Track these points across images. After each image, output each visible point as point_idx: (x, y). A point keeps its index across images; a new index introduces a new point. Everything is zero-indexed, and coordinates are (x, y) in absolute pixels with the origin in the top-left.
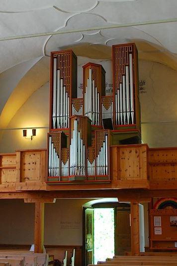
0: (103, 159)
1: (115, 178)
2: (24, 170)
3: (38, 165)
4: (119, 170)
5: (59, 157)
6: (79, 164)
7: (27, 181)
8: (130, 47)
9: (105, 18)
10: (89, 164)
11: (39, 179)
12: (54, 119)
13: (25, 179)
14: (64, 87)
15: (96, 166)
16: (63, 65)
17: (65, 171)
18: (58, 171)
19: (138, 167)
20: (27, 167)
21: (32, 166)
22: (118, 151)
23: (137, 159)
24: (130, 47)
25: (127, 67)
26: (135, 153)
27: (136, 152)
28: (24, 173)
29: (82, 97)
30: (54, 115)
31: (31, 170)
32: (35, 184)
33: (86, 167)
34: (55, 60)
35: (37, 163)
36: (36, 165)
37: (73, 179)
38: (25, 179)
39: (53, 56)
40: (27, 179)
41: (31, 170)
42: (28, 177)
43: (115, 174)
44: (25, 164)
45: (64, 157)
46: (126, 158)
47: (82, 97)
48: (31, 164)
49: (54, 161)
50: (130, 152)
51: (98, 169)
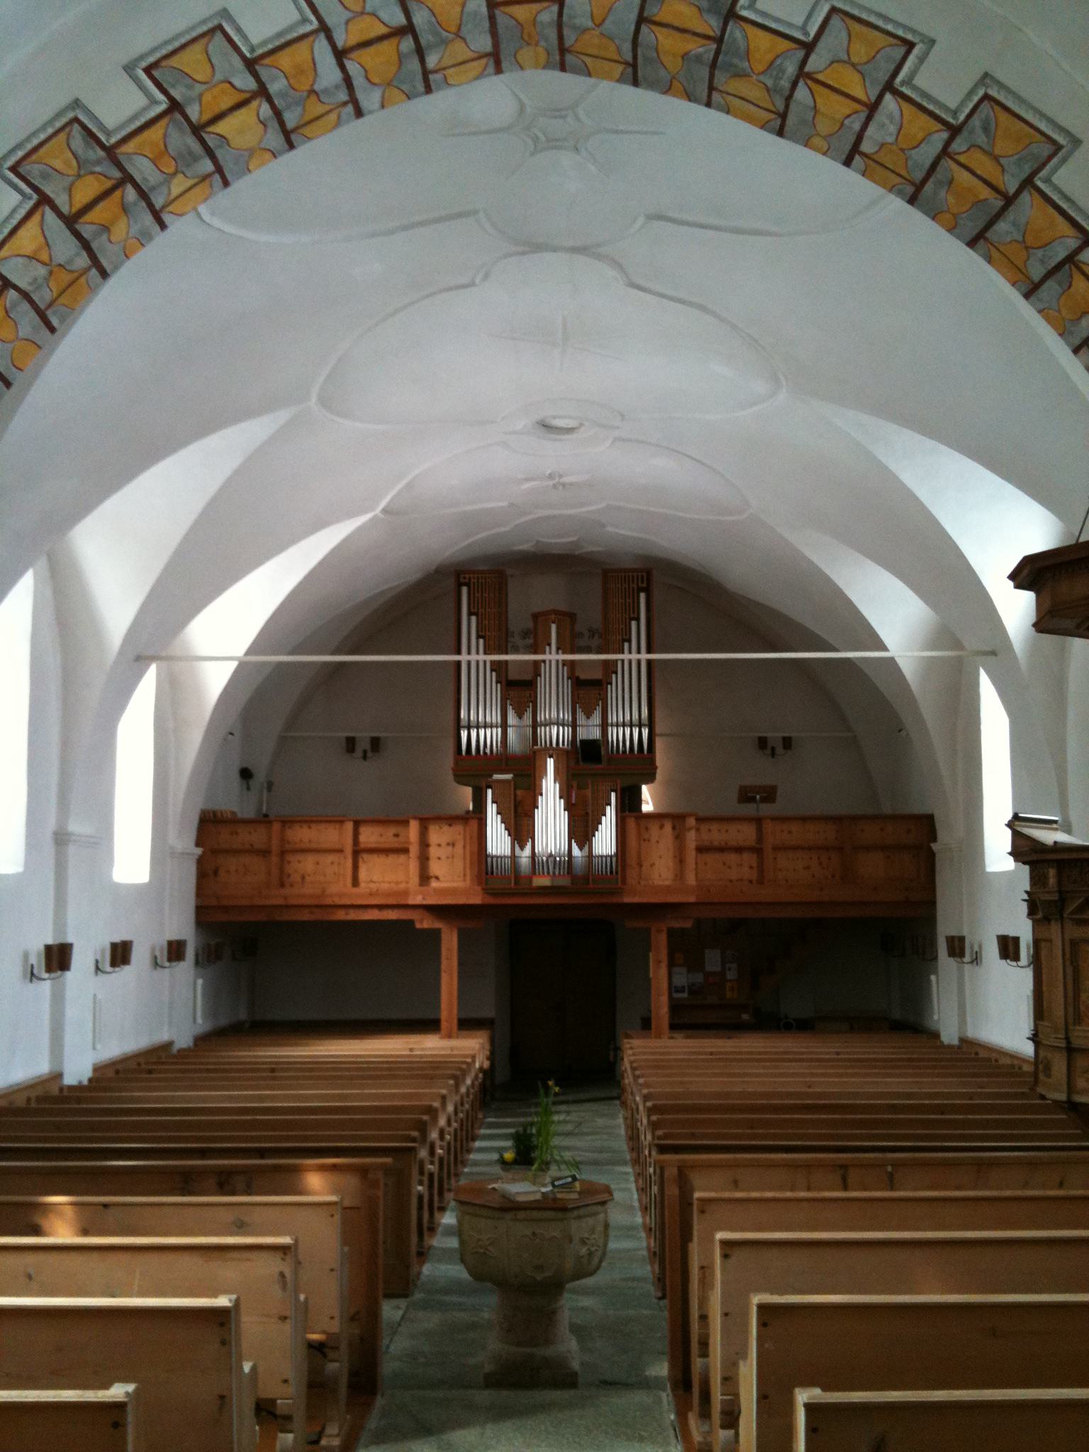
0: (605, 841)
27: (674, 828)
45: (521, 828)
46: (654, 839)
49: (498, 840)
50: (662, 827)
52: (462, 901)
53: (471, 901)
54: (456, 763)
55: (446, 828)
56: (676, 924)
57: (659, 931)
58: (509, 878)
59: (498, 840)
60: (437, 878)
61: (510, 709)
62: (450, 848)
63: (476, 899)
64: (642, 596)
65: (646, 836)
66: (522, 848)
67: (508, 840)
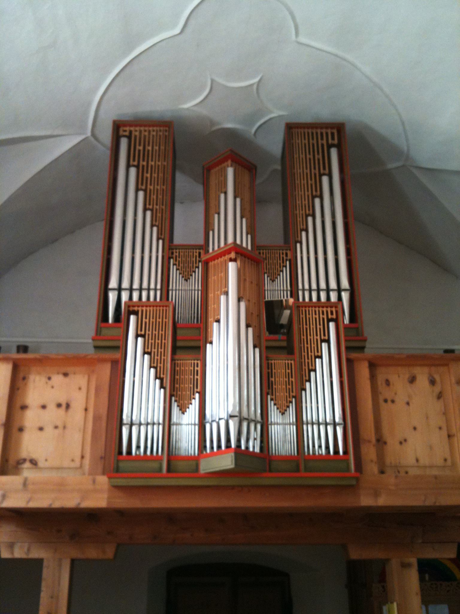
0: (324, 397)
1: (371, 468)
2: (21, 430)
3: (77, 415)
4: (380, 441)
5: (162, 386)
6: (245, 409)
7: (27, 472)
8: (333, 134)
9: (298, 20)
10: (274, 415)
11: (77, 463)
12: (112, 297)
13: (21, 462)
14: (149, 213)
15: (299, 423)
16: (146, 155)
17: (186, 438)
18: (158, 431)
19: (444, 433)
20: (31, 418)
21: (53, 415)
22: (373, 377)
23: (439, 406)
24: (333, 134)
25: (325, 179)
26: (426, 383)
27: (433, 382)
28: (18, 443)
29: (201, 242)
30: (113, 283)
31: (49, 430)
32: (61, 487)
33: (265, 424)
34: (124, 142)
35: (73, 405)
36: (71, 410)
37: (227, 462)
38: (21, 462)
39: (118, 127)
40: (27, 465)
41: (49, 430)
42: (34, 456)
43: (369, 452)
44: (24, 407)
45: (182, 382)
46: (401, 398)
47: (201, 242)
48: (52, 407)
49: (143, 396)
50: (412, 380)
51: (309, 431)
52: (70, 501)
53: (89, 503)
54: (98, 331)
55: (57, 379)
56: (430, 554)
57: (405, 566)
58: (158, 459)
59: (143, 396)
60: (34, 462)
61: (173, 270)
62: (61, 411)
63: (99, 501)
64: (334, 153)
65: (389, 396)
66: (183, 410)
67: (160, 395)
